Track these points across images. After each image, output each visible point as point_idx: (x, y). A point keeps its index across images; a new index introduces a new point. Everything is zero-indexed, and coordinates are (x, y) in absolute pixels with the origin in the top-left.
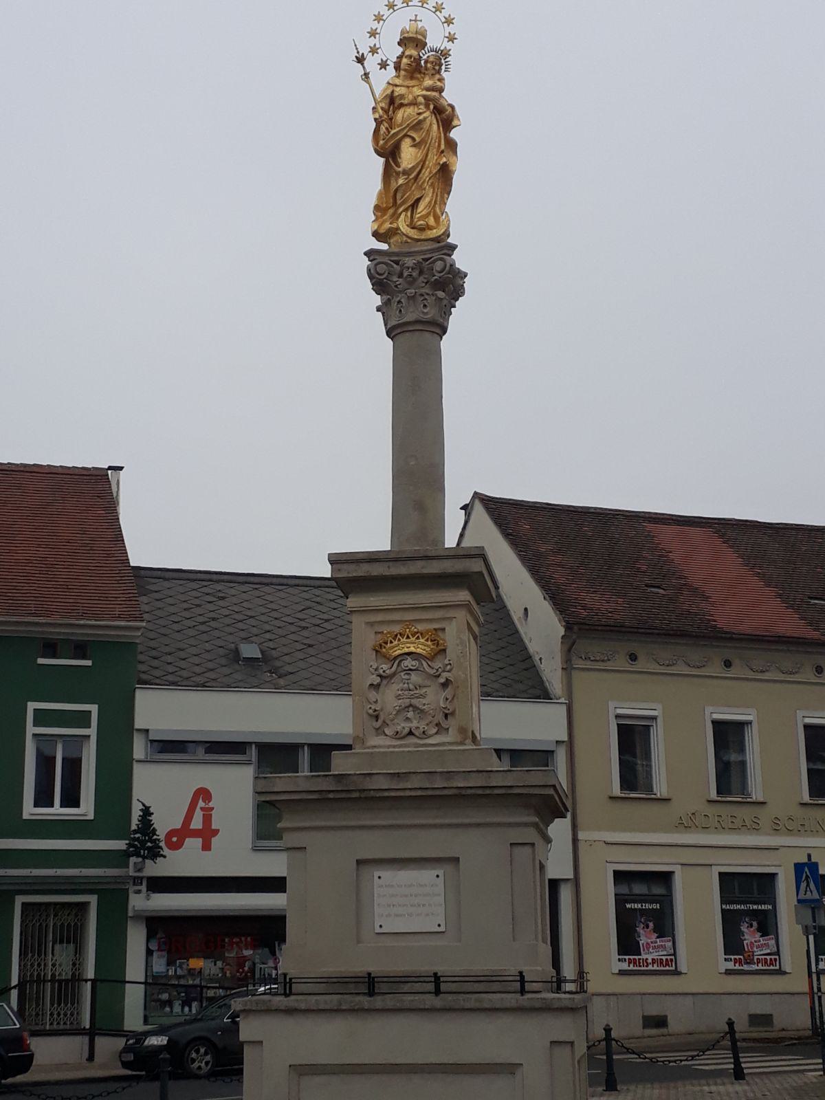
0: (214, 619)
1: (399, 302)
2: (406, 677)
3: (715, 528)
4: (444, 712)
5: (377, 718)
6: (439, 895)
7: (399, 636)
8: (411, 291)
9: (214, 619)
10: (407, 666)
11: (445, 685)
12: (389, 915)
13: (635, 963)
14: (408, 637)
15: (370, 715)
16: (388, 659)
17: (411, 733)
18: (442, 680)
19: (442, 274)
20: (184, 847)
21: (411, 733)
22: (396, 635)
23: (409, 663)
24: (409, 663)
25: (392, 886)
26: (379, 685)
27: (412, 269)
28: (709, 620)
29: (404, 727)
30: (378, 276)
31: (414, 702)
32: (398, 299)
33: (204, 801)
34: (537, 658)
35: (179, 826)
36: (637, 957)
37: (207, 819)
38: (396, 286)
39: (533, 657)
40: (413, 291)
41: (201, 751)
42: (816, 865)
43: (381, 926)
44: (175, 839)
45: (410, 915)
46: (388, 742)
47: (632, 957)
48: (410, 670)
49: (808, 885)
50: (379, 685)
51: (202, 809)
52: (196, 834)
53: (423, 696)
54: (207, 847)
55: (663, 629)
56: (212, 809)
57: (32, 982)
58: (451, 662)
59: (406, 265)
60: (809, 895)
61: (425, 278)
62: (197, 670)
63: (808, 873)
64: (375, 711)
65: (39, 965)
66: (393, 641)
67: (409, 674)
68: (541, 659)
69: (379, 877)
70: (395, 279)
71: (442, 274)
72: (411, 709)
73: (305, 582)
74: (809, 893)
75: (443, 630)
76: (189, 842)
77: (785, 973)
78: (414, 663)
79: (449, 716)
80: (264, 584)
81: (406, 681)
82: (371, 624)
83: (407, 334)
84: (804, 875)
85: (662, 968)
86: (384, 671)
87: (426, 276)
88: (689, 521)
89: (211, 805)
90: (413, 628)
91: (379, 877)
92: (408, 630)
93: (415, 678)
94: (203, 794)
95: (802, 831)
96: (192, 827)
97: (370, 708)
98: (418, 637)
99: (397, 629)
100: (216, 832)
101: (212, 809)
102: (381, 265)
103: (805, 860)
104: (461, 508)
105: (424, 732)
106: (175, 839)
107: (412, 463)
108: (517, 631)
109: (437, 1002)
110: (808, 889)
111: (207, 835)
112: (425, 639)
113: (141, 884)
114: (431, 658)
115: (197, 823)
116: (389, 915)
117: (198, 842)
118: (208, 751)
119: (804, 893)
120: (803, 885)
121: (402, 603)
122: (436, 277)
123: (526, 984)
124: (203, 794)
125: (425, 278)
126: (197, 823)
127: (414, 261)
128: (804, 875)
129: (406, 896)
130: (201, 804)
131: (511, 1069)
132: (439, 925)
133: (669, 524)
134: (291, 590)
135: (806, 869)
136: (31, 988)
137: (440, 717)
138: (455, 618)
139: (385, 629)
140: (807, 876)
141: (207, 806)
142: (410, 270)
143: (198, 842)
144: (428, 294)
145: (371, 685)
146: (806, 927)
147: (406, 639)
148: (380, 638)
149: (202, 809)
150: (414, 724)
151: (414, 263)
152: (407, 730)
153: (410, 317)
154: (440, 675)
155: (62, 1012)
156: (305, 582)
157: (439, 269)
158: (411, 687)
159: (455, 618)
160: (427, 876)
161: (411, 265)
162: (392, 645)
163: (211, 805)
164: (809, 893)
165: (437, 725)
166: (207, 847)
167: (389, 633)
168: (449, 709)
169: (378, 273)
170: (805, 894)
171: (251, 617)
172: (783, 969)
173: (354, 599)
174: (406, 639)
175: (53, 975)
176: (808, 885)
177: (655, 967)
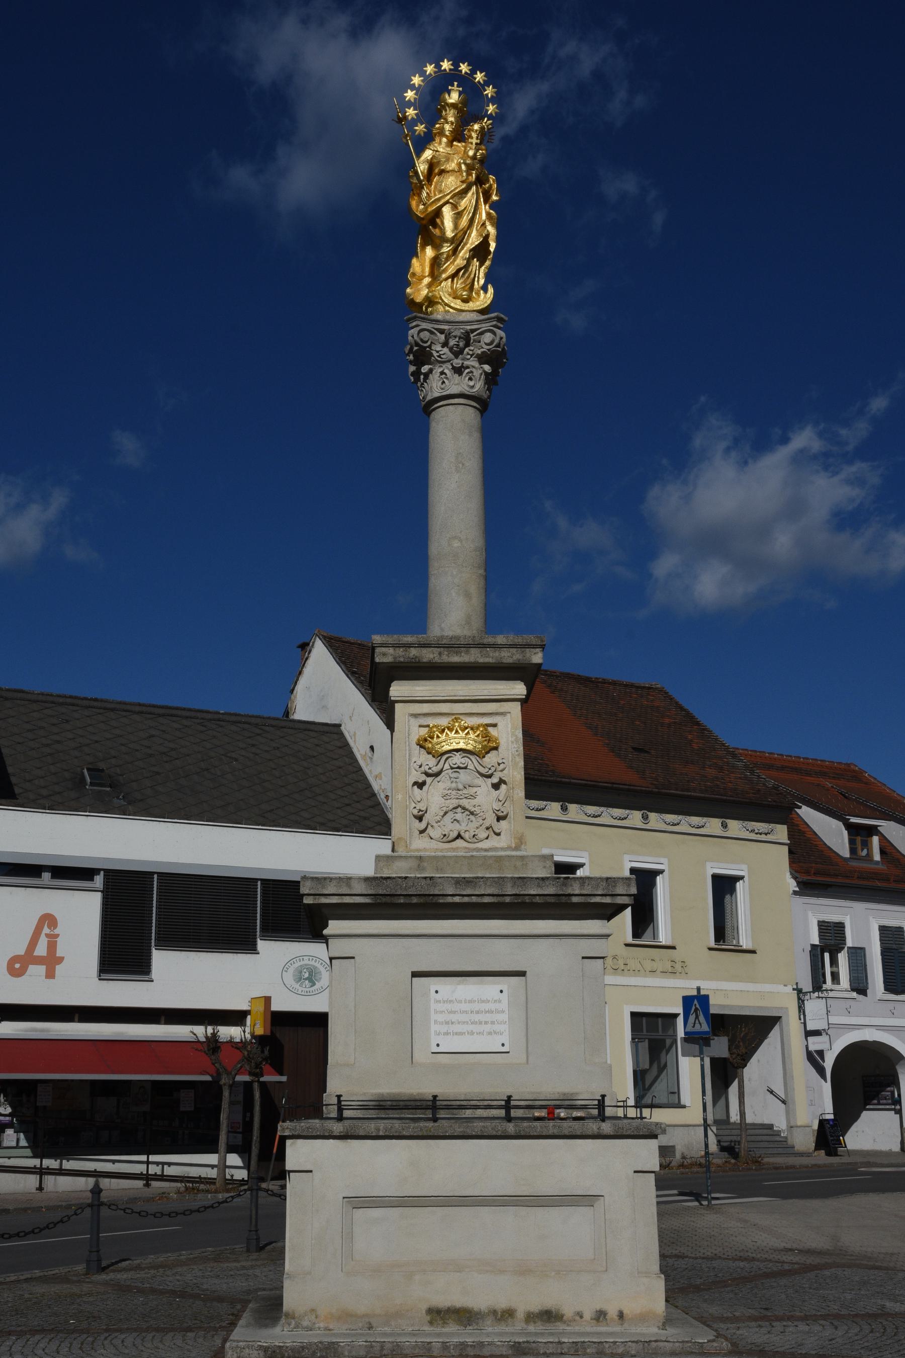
0: (58, 742)
1: (442, 373)
2: (455, 775)
4: (496, 815)
5: (420, 819)
6: (503, 1012)
7: (446, 730)
8: (457, 362)
9: (58, 742)
10: (456, 764)
11: (496, 786)
12: (447, 1034)
14: (457, 732)
15: (415, 817)
17: (459, 836)
18: (495, 780)
19: (491, 347)
20: (27, 973)
21: (459, 836)
23: (457, 759)
24: (457, 759)
25: (451, 1001)
26: (424, 783)
27: (459, 339)
29: (452, 829)
30: (421, 344)
31: (465, 803)
32: (441, 369)
33: (49, 927)
34: (383, 796)
35: (21, 951)
37: (52, 946)
38: (439, 356)
39: (378, 795)
40: (461, 362)
41: (46, 876)
42: (706, 997)
43: (438, 1045)
44: (17, 966)
45: (472, 1033)
46: (434, 845)
48: (459, 768)
49: (697, 1017)
50: (424, 783)
51: (47, 935)
52: (39, 961)
53: (473, 797)
54: (50, 975)
56: (57, 936)
58: (504, 761)
59: (453, 334)
60: (698, 1028)
61: (470, 350)
62: (44, 792)
63: (698, 1006)
64: (420, 810)
66: (440, 735)
67: (458, 772)
68: (387, 797)
69: (437, 992)
70: (439, 348)
71: (491, 347)
72: (459, 810)
74: (697, 1025)
75: (495, 725)
76: (33, 969)
77: (684, 1107)
78: (463, 760)
80: (108, 709)
81: (455, 780)
82: (416, 716)
83: (450, 407)
84: (694, 1008)
86: (430, 768)
87: (472, 348)
89: (56, 931)
90: (462, 722)
91: (501, 991)
92: (457, 724)
93: (463, 776)
94: (49, 920)
95: (626, 970)
96: (37, 953)
97: (415, 808)
98: (468, 732)
99: (444, 722)
100: (61, 960)
101: (57, 936)
102: (426, 332)
103: (695, 993)
104: (299, 647)
105: (474, 836)
106: (17, 966)
107: (456, 545)
108: (361, 769)
109: (511, 1128)
110: (697, 1022)
111: (52, 962)
112: (476, 735)
114: (480, 754)
115: (41, 950)
116: (447, 1034)
117: (42, 969)
118: (54, 876)
119: (692, 1025)
120: (692, 1018)
121: (453, 694)
122: (485, 350)
123: (606, 1108)
124: (49, 920)
125: (470, 350)
126: (41, 950)
127: (462, 331)
128: (694, 1008)
129: (466, 1012)
130: (46, 930)
131: (588, 1200)
132: (503, 1045)
135: (696, 1002)
137: (491, 819)
138: (510, 713)
139: (432, 722)
140: (696, 1009)
141: (52, 933)
142: (457, 339)
143: (42, 969)
144: (473, 367)
145: (415, 783)
147: (455, 733)
148: (424, 732)
149: (47, 935)
150: (462, 828)
151: (462, 333)
152: (455, 834)
153: (454, 390)
157: (488, 341)
158: (461, 787)
159: (510, 713)
160: (490, 989)
161: (459, 334)
163: (56, 931)
165: (487, 828)
166: (50, 975)
167: (435, 726)
168: (503, 812)
169: (422, 340)
170: (694, 1027)
171: (97, 742)
172: (682, 1103)
173: (398, 688)
174: (455, 733)
176: (697, 1017)
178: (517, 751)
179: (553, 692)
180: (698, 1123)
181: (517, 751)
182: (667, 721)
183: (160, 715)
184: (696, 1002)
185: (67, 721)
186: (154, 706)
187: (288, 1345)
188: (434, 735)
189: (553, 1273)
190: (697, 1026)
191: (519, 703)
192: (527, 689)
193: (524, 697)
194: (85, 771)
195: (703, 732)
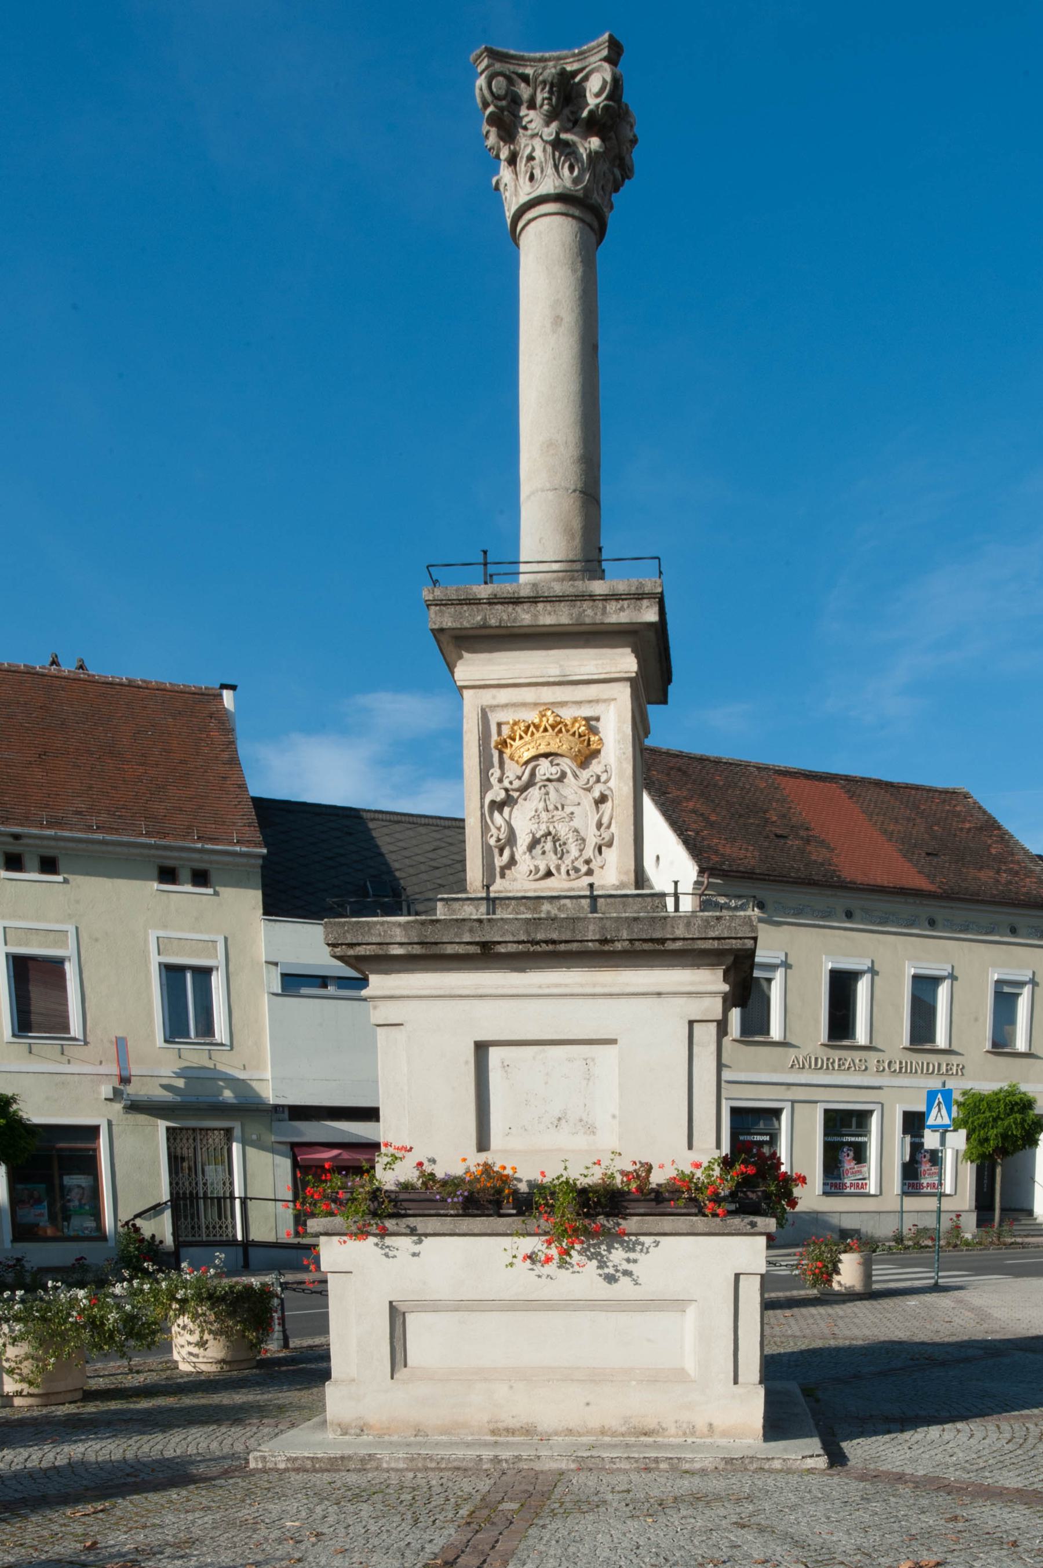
3: (841, 784)
7: (532, 728)
13: (836, 1187)
16: (517, 762)
22: (528, 727)
28: (834, 870)
36: (915, 1182)
47: (911, 1182)
49: (939, 1110)
55: (791, 877)
57: (185, 1198)
63: (941, 1100)
65: (177, 1184)
73: (434, 821)
74: (939, 1118)
79: (604, 848)
84: (937, 1102)
85: (858, 1191)
88: (816, 776)
113: (283, 1112)
128: (937, 1102)
133: (797, 778)
134: (422, 830)
135: (939, 1096)
136: (225, 1202)
140: (939, 1103)
146: (957, 1151)
154: (592, 787)
155: (211, 1229)
156: (434, 821)
162: (522, 741)
164: (939, 1118)
175: (205, 1193)
176: (939, 1110)
177: (852, 1190)
178: (624, 753)
179: (850, 798)
180: (896, 1210)
181: (624, 753)
182: (967, 826)
183: (445, 827)
184: (939, 1096)
185: (350, 834)
186: (440, 818)
187: (319, 1456)
188: (515, 735)
189: (634, 1383)
190: (939, 1119)
191: (628, 684)
192: (636, 657)
193: (634, 675)
194: (368, 884)
195: (1004, 837)
